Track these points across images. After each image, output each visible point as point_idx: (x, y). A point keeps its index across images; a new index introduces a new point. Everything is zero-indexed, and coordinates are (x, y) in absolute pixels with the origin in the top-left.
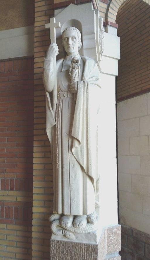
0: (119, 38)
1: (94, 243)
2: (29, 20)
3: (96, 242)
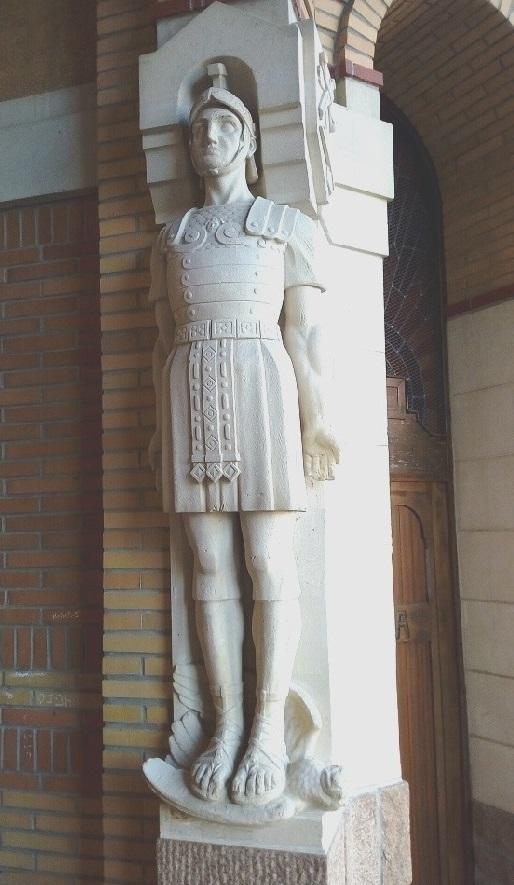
0: (388, 129)
1: (312, 851)
2: (80, 73)
3: (319, 845)
